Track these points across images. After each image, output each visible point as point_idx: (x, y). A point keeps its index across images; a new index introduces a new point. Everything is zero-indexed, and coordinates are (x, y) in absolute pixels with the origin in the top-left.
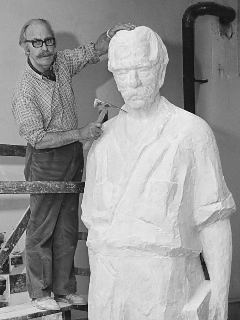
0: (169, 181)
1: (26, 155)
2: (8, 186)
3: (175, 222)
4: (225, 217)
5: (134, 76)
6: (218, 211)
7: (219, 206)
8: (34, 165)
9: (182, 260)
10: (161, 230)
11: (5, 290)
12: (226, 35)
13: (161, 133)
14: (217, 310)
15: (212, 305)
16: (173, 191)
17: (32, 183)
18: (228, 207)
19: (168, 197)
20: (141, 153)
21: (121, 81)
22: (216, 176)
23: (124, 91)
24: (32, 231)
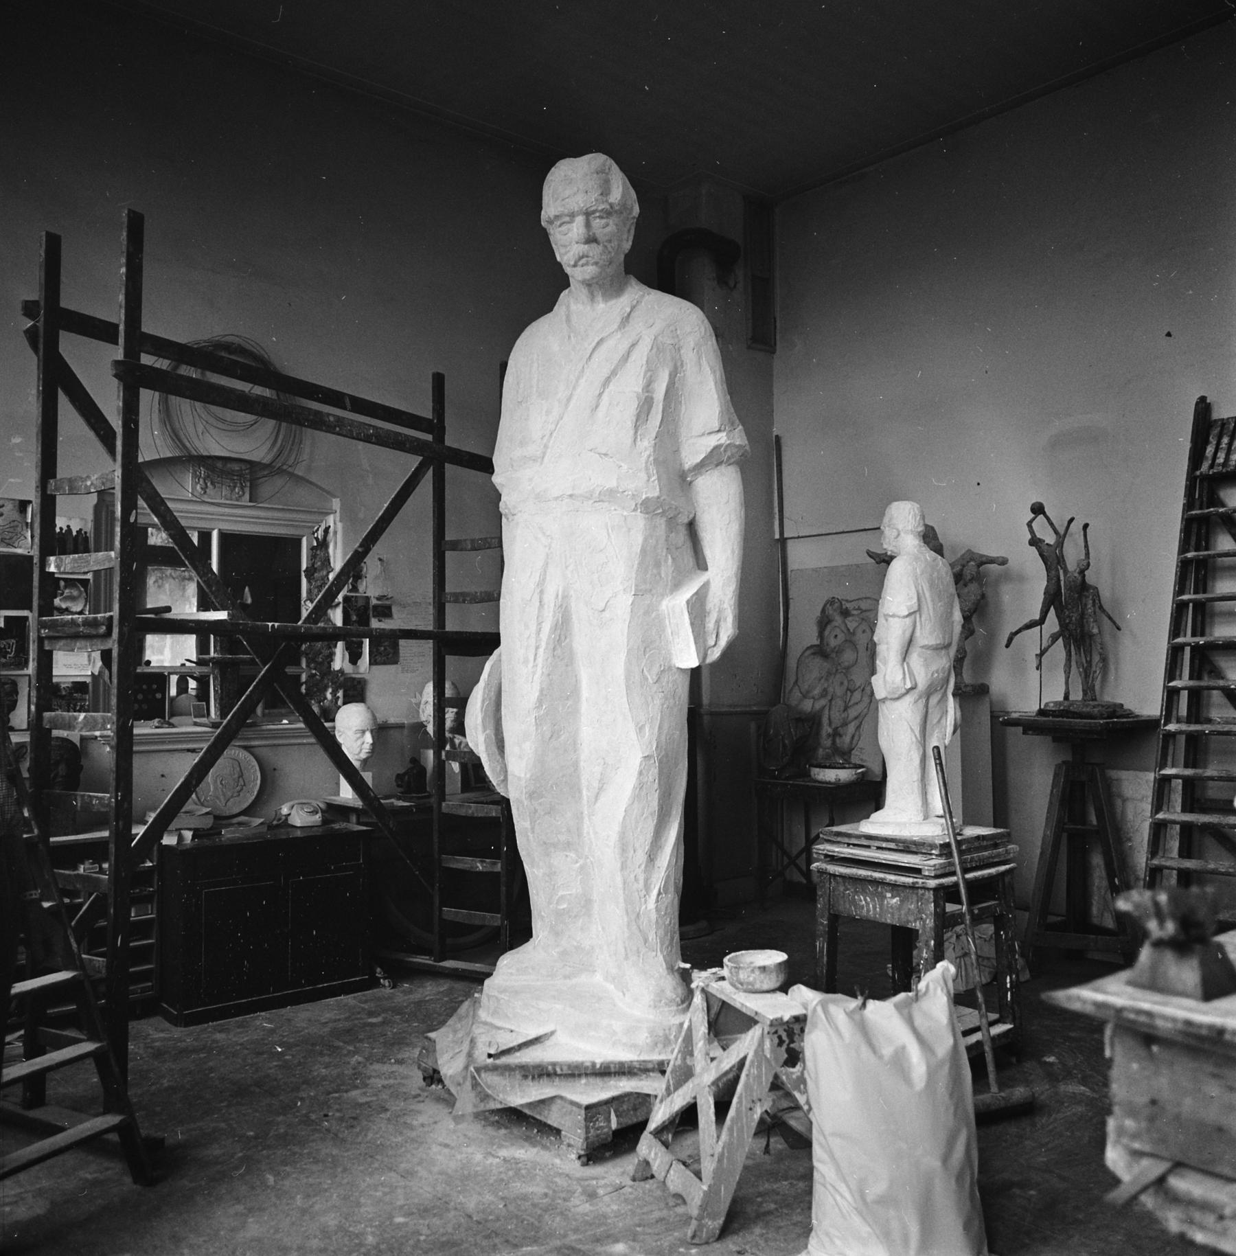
0: (640, 391)
3: (649, 456)
4: (732, 460)
7: (722, 438)
9: (661, 523)
10: (625, 467)
14: (720, 612)
15: (712, 602)
16: (646, 407)
20: (594, 350)
21: (564, 237)
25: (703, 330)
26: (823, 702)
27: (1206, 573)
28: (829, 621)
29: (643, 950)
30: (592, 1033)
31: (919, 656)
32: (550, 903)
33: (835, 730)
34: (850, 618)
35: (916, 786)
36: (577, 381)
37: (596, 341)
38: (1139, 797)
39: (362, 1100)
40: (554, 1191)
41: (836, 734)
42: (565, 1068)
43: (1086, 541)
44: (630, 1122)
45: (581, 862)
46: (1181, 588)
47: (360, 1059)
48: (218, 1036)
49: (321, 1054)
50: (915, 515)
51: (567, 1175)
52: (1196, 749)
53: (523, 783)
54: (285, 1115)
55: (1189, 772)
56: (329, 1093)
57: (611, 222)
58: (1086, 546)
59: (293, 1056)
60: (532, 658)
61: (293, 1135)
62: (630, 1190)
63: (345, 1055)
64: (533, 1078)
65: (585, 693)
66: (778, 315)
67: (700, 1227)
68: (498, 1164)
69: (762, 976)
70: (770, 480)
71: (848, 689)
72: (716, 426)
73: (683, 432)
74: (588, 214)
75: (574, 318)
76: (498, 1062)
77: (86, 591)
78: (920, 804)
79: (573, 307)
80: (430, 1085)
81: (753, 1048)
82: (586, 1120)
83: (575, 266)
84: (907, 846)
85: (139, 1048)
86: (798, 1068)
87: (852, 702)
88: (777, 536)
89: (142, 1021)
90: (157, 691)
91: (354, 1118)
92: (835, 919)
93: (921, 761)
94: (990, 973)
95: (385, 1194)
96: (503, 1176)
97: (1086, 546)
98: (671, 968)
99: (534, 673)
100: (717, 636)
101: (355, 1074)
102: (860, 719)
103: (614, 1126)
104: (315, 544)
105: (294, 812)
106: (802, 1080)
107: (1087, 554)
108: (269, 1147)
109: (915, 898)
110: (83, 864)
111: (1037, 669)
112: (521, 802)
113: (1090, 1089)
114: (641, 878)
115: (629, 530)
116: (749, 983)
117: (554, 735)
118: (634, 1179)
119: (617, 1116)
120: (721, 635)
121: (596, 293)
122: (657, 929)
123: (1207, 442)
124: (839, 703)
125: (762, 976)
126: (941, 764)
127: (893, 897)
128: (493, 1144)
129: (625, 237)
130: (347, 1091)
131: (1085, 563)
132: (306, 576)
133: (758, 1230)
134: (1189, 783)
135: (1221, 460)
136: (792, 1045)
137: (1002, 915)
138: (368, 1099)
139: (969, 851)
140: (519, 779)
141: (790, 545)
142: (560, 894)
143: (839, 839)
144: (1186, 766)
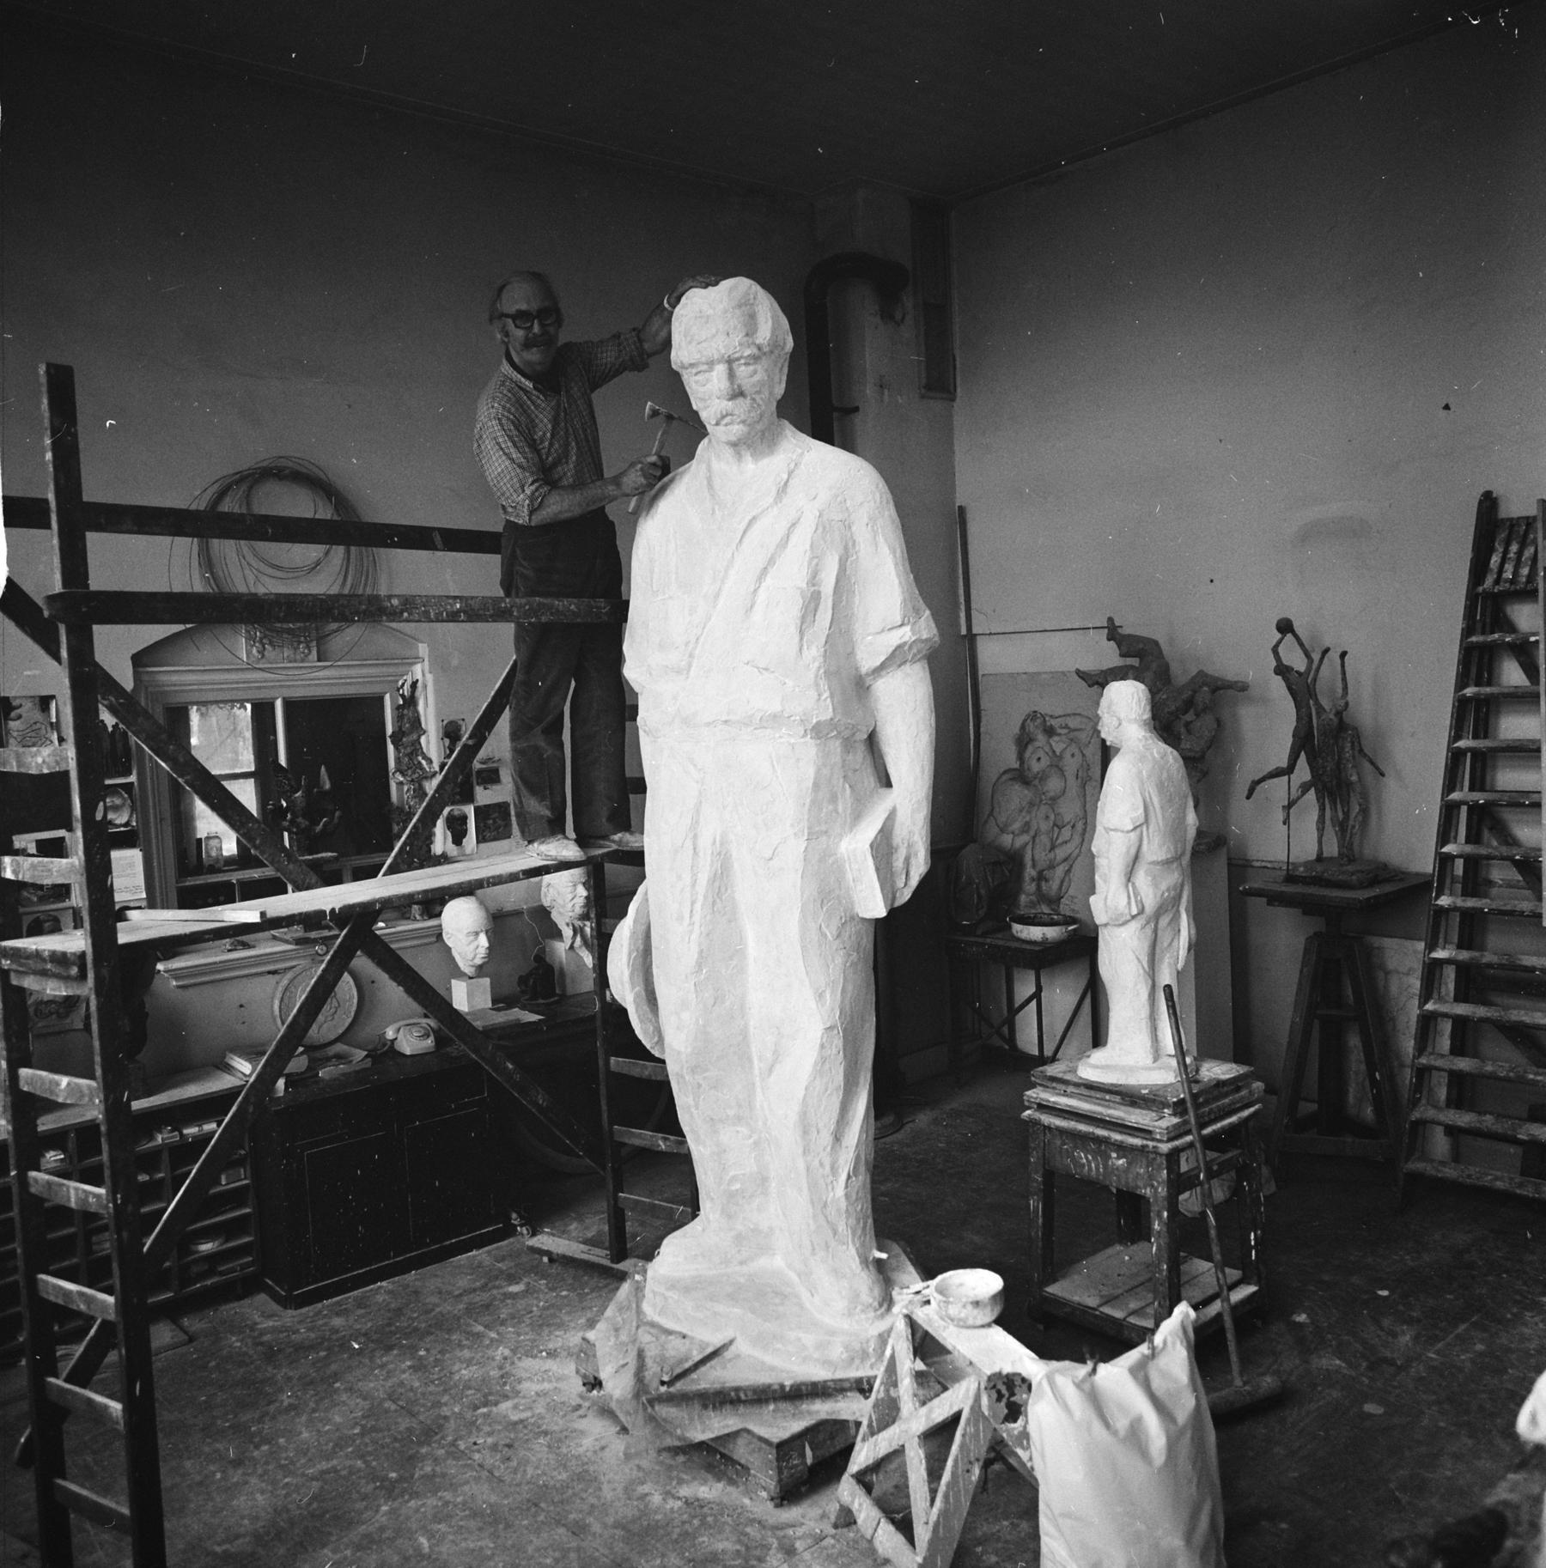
1: (503, 550)
2: (477, 606)
3: (819, 668)
5: (724, 376)
6: (905, 643)
7: (905, 634)
8: (522, 565)
9: (836, 746)
10: (790, 683)
11: (465, 836)
12: (892, 317)
13: (783, 489)
14: (909, 846)
15: (900, 834)
16: (813, 605)
17: (524, 601)
18: (925, 637)
19: (803, 619)
20: (745, 532)
21: (702, 389)
22: (898, 576)
23: (706, 408)
24: (522, 703)
25: (878, 496)
26: (1025, 838)
27: (1488, 711)
28: (1031, 740)
29: (833, 1244)
30: (779, 1346)
31: (1146, 873)
33: (1040, 873)
34: (1056, 738)
35: (1144, 1025)
36: (726, 571)
37: (746, 521)
38: (1405, 971)
39: (515, 1417)
40: (748, 1548)
41: (1041, 878)
42: (749, 1393)
45: (755, 1137)
46: (1457, 732)
47: (507, 1352)
48: (337, 1322)
49: (460, 1346)
51: (759, 1522)
52: (1472, 928)
53: (683, 1057)
54: (429, 1445)
55: (1464, 955)
56: (476, 1408)
57: (759, 367)
58: (1344, 679)
59: (427, 1350)
60: (687, 916)
62: (832, 1541)
63: (488, 1347)
65: (752, 949)
66: (957, 353)
68: (680, 1508)
69: (976, 1312)
70: (954, 554)
71: (1055, 825)
73: (858, 628)
74: (730, 362)
75: (717, 482)
76: (672, 1389)
77: (131, 796)
78: (1149, 1044)
79: (715, 465)
80: (590, 1391)
81: (970, 1402)
82: (778, 1460)
83: (717, 424)
84: (1130, 1097)
85: (246, 1345)
86: (1020, 1422)
87: (1059, 841)
88: (964, 631)
89: (247, 1301)
91: (509, 1446)
92: (1049, 1175)
93: (1149, 996)
94: (1229, 1187)
96: (687, 1526)
98: (865, 1261)
99: (691, 932)
101: (502, 1377)
103: (809, 1461)
104: (401, 702)
105: (400, 1036)
106: (1025, 1435)
107: (1345, 688)
108: (415, 1495)
109: (1144, 1161)
110: (161, 1133)
111: (1284, 823)
112: (682, 1077)
114: (827, 1162)
115: (798, 760)
116: (960, 1320)
117: (718, 1000)
118: (836, 1526)
119: (812, 1449)
121: (743, 452)
122: (847, 1218)
123: (1491, 550)
124: (1044, 840)
126: (1175, 1013)
127: (1119, 1158)
128: (671, 1479)
129: (777, 379)
130: (496, 1404)
131: (1342, 703)
132: (393, 743)
134: (1463, 969)
135: (1508, 575)
136: (1012, 1399)
138: (523, 1415)
139: (1207, 1102)
140: (679, 1053)
142: (731, 1174)
143: (1054, 1085)
144: (1460, 946)
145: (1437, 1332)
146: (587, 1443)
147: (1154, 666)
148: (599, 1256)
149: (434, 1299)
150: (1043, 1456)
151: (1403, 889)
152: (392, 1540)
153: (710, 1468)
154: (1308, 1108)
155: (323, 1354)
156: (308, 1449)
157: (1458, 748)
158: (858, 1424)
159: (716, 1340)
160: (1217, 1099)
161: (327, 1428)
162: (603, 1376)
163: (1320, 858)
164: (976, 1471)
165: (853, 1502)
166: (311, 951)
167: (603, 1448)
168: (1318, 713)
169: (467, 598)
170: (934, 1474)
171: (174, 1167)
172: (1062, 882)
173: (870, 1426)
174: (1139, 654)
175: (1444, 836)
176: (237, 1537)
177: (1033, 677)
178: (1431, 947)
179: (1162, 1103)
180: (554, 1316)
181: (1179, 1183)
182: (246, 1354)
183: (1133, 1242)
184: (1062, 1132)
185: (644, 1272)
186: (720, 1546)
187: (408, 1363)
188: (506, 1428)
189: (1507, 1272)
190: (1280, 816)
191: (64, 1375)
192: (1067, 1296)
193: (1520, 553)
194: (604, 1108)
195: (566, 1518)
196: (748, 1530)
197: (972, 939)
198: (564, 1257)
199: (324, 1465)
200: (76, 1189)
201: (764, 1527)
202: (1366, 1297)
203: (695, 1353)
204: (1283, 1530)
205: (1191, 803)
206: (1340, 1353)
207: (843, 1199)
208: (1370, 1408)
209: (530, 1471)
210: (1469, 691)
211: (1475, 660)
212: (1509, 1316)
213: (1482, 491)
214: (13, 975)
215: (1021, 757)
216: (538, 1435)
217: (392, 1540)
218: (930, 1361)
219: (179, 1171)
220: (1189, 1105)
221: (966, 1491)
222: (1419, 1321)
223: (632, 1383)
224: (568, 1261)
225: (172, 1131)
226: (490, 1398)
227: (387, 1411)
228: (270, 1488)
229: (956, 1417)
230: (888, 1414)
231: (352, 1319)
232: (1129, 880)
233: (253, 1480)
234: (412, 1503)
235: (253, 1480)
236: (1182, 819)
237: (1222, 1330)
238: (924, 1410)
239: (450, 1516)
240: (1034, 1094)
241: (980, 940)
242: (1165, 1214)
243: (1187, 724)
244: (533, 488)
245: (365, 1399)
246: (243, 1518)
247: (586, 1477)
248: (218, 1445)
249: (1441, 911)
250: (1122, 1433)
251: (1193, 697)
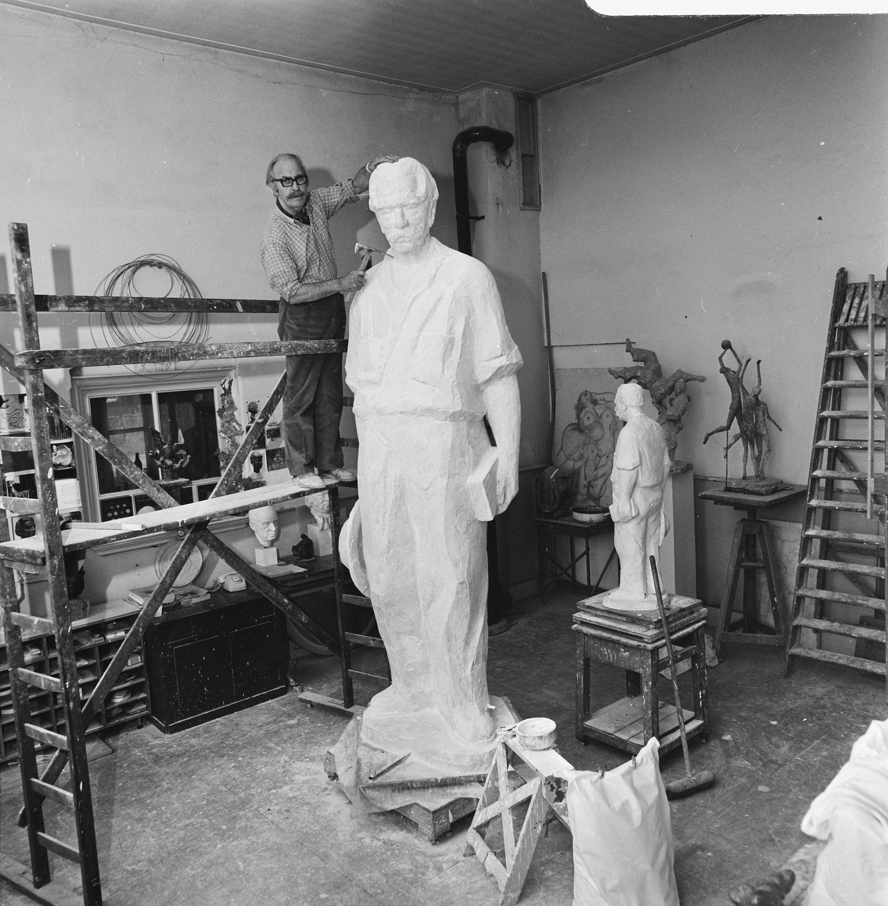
0: (445, 334)
3: (454, 382)
6: (503, 366)
7: (503, 361)
8: (289, 322)
9: (464, 425)
12: (504, 164)
14: (506, 481)
16: (450, 345)
17: (287, 343)
18: (514, 362)
19: (445, 353)
23: (388, 233)
26: (580, 463)
28: (584, 407)
30: (435, 758)
32: (402, 668)
33: (589, 482)
34: (598, 406)
35: (640, 578)
37: (413, 297)
39: (291, 795)
40: (416, 867)
41: (589, 485)
43: (759, 372)
44: (461, 816)
45: (421, 642)
46: (823, 407)
47: (287, 758)
48: (194, 741)
49: (261, 755)
50: (638, 395)
55: (825, 533)
56: (270, 790)
58: (759, 376)
59: (243, 757)
60: (381, 518)
61: (251, 827)
62: (463, 864)
64: (399, 790)
67: (506, 898)
71: (597, 455)
72: (499, 353)
76: (376, 782)
84: (632, 619)
87: (600, 465)
90: (126, 508)
91: (288, 811)
92: (587, 661)
95: (313, 875)
97: (759, 376)
98: (482, 711)
99: (384, 529)
100: (505, 496)
101: (284, 772)
102: (606, 476)
103: (451, 820)
106: (566, 808)
107: (760, 381)
113: (751, 763)
114: (461, 656)
120: (507, 495)
122: (473, 687)
123: (844, 302)
124: (591, 465)
125: (540, 742)
126: (655, 568)
127: (625, 652)
128: (376, 829)
130: (281, 787)
131: (758, 390)
133: (541, 894)
135: (853, 316)
137: (697, 654)
138: (296, 794)
139: (674, 621)
140: (378, 596)
141: (555, 351)
142: (409, 662)
143: (589, 610)
144: (823, 528)
145: (803, 746)
146: (331, 809)
147: (652, 367)
148: (338, 704)
149: (247, 728)
150: (574, 821)
151: (791, 495)
152: (224, 863)
153: (397, 823)
154: (737, 616)
155: (186, 759)
156: (178, 813)
157: (823, 416)
158: (478, 800)
159: (400, 755)
160: (679, 618)
161: (188, 801)
162: (338, 773)
163: (745, 478)
164: (540, 828)
165: (474, 843)
166: (174, 535)
167: (339, 812)
168: (743, 394)
169: (255, 344)
170: (518, 826)
171: (102, 656)
172: (601, 488)
173: (484, 801)
174: (644, 360)
175: (815, 466)
176: (139, 862)
177: (586, 371)
178: (806, 528)
179: (648, 621)
180: (312, 738)
181: (658, 666)
182: (143, 759)
183: (635, 696)
184: (594, 637)
185: (362, 714)
186: (401, 867)
187: (233, 765)
188: (286, 801)
189: (843, 710)
190: (723, 453)
191: (42, 778)
192: (597, 727)
193: (860, 304)
194: (340, 622)
195: (318, 851)
196: (417, 857)
197: (551, 521)
198: (319, 704)
199: (187, 822)
200: (45, 679)
201: (426, 856)
202: (764, 725)
203: (389, 761)
204: (709, 857)
205: (666, 453)
206: (747, 756)
207: (470, 677)
208: (761, 788)
209: (299, 825)
210: (830, 383)
211: (834, 364)
212: (843, 736)
213: (839, 269)
214: (5, 562)
215: (578, 417)
216: (303, 805)
217: (224, 863)
218: (517, 767)
219: (104, 659)
220: (663, 623)
221: (534, 839)
222: (792, 739)
223: (354, 777)
224: (321, 708)
225: (100, 637)
226: (277, 784)
227: (221, 791)
228: (157, 834)
229: (529, 799)
230: (494, 796)
231: (202, 739)
232: (631, 497)
233: (148, 830)
234: (234, 843)
235: (148, 830)
236: (661, 462)
237: (681, 747)
238: (511, 795)
239: (254, 850)
240: (579, 615)
241: (556, 521)
242: (650, 683)
243: (671, 400)
244: (292, 285)
245: (209, 785)
246: (142, 851)
247: (329, 828)
248: (128, 811)
249: (812, 509)
250: (617, 809)
251: (674, 385)
